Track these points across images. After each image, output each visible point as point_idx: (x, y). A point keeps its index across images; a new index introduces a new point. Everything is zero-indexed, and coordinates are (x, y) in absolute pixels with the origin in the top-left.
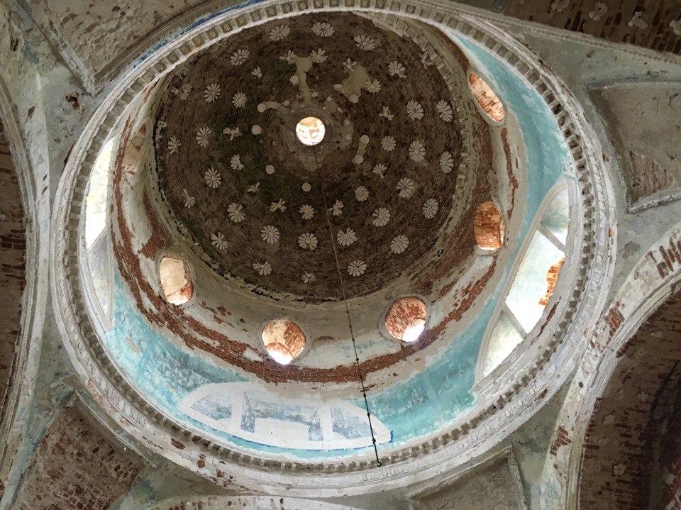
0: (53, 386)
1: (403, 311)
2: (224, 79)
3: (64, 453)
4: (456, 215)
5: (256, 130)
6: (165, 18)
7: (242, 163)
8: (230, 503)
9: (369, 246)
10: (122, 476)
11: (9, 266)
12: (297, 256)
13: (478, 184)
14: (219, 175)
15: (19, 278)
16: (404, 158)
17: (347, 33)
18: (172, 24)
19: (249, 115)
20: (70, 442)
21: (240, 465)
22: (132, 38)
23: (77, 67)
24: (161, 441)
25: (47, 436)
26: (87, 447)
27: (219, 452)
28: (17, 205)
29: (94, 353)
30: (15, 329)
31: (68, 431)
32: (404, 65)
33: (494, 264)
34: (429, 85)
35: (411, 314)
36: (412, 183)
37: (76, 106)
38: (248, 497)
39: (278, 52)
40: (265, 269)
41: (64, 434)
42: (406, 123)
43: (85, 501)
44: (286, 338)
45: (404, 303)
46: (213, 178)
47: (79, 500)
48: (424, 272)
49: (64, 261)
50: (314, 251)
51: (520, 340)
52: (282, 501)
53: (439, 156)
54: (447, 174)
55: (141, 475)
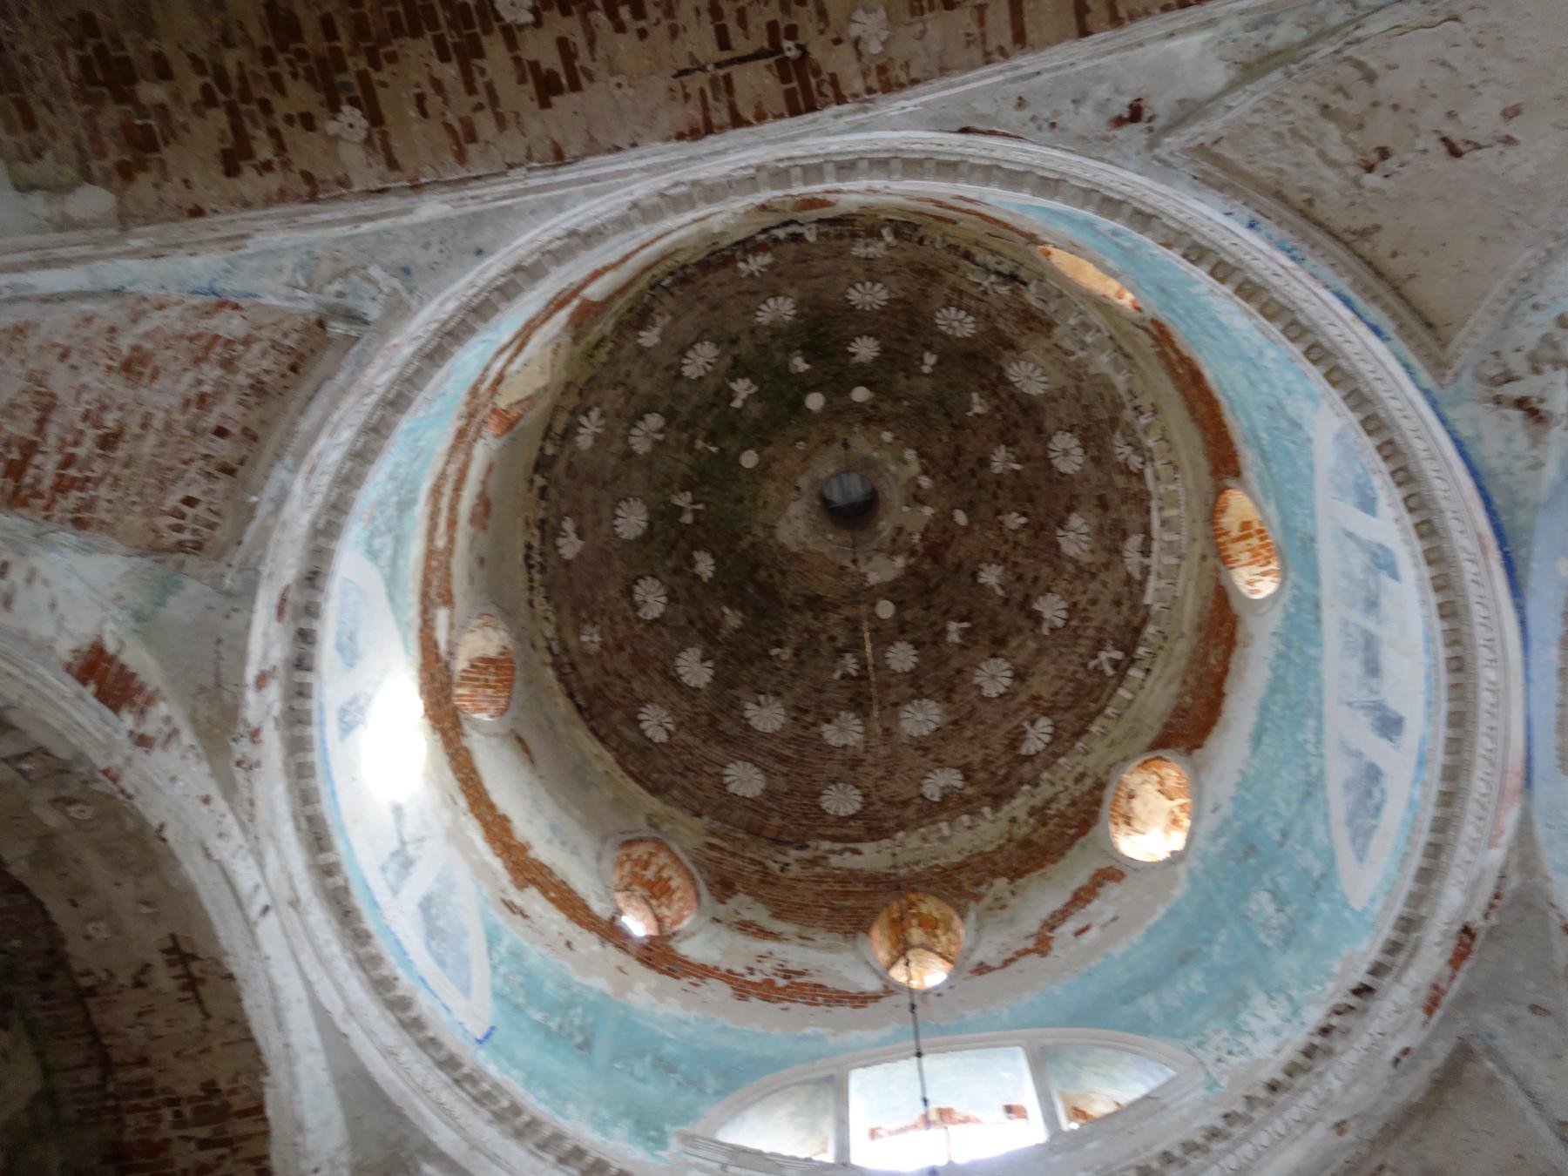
0: (375, 272)
1: (646, 866)
2: (898, 307)
3: (197, 361)
4: (872, 857)
5: (815, 401)
6: (1365, 248)
7: (745, 401)
8: (207, 800)
9: (703, 720)
10: (174, 521)
11: (730, 90)
12: (614, 593)
13: (960, 867)
14: (709, 368)
15: (707, 121)
16: (893, 698)
17: (1076, 497)
18: (1354, 264)
19: (838, 377)
20: (228, 364)
21: (286, 764)
22: (1306, 196)
23: (1230, 108)
24: (284, 565)
25: (236, 307)
26: (228, 409)
27: (296, 703)
28: (914, 74)
29: (453, 324)
30: (570, 151)
31: (256, 348)
32: (1067, 620)
33: (876, 998)
34: (1060, 683)
35: (649, 885)
36: (858, 737)
37: (1119, 122)
38: (236, 831)
39: (983, 387)
40: (570, 547)
41: (247, 342)
42: (959, 671)
43: (86, 465)
44: (473, 666)
45: (662, 859)
46: (700, 361)
47: (81, 452)
48: (738, 861)
49: (676, 184)
50: (638, 620)
51: (829, 1157)
52: (266, 909)
53: (940, 763)
54: (922, 796)
55: (192, 562)
